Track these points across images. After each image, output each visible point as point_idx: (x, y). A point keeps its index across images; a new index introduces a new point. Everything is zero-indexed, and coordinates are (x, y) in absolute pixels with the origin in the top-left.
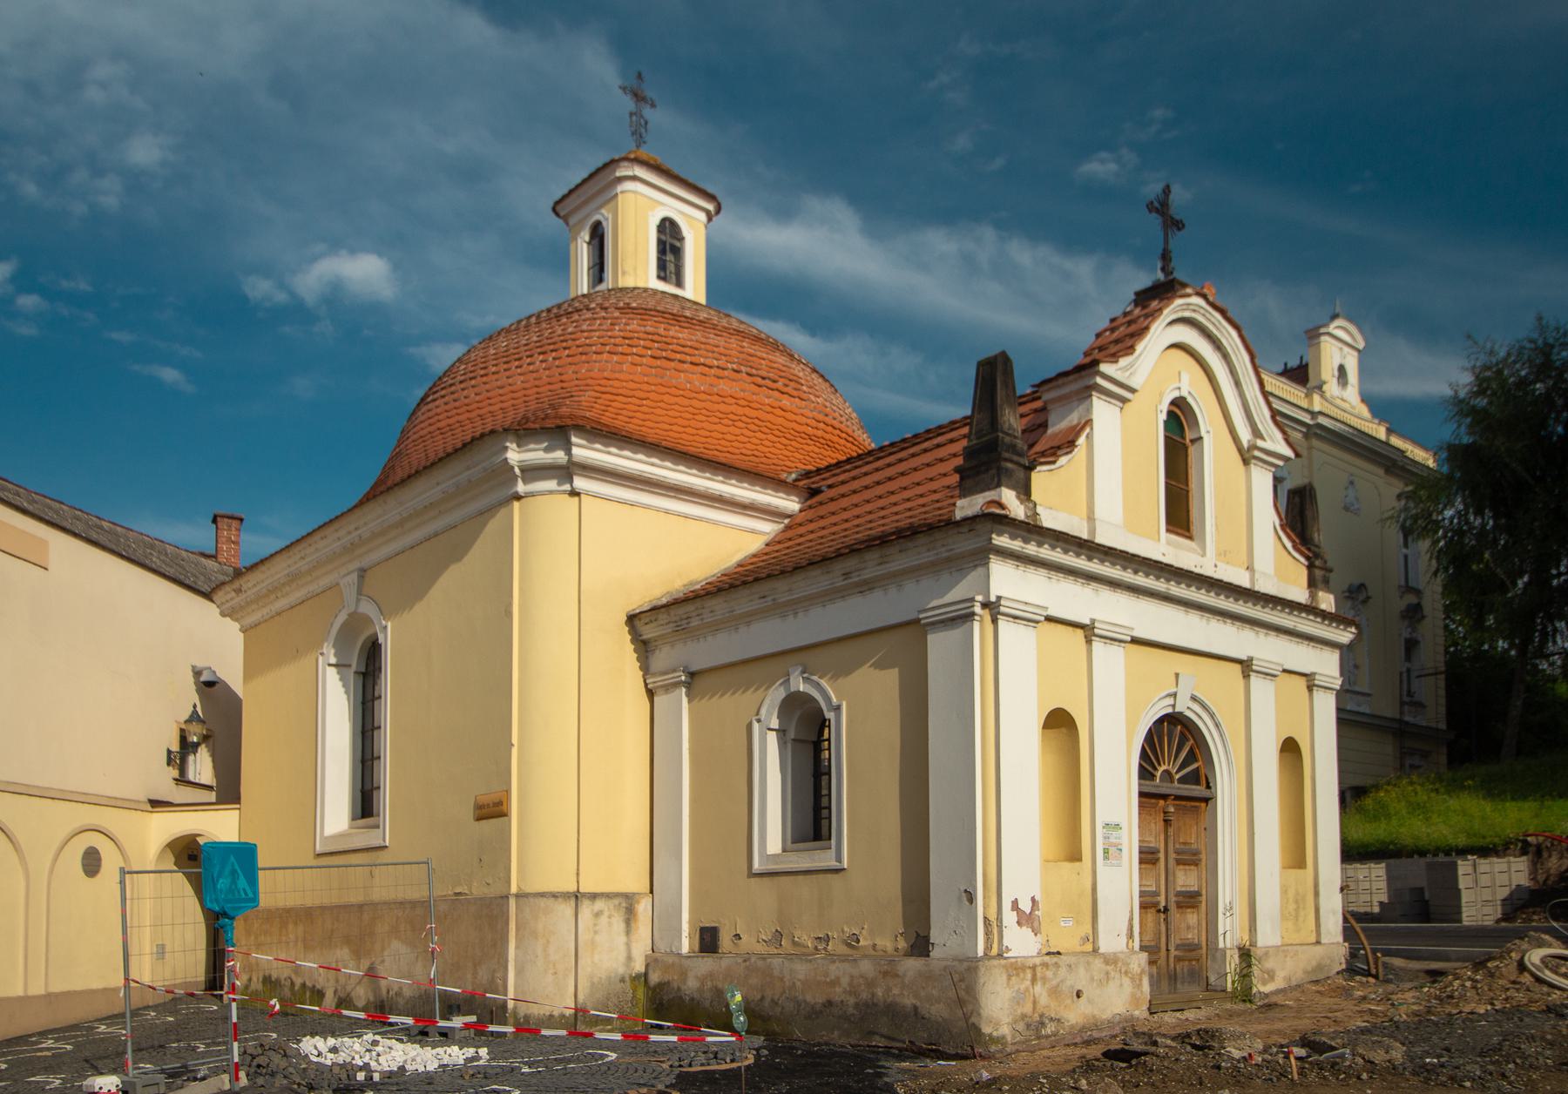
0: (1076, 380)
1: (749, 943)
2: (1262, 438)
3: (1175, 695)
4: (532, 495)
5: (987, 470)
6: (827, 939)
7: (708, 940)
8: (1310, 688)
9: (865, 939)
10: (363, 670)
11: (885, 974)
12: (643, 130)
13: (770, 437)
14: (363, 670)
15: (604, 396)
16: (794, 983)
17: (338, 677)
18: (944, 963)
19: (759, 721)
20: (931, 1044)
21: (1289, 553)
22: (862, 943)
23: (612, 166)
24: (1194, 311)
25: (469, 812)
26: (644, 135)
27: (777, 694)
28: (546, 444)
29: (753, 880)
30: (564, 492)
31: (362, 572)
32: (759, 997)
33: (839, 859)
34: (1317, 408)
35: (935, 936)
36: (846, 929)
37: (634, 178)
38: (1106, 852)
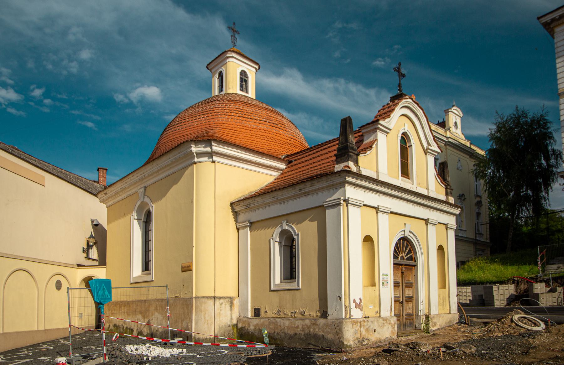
0: (372, 126)
1: (270, 314)
2: (431, 146)
3: (404, 231)
4: (200, 162)
5: (344, 156)
6: (295, 312)
7: (257, 313)
8: (447, 229)
9: (307, 312)
10: (146, 221)
11: (313, 324)
12: (235, 41)
13: (276, 143)
14: (146, 221)
15: (223, 129)
16: (284, 327)
17: (137, 223)
18: (332, 321)
19: (273, 239)
20: (328, 348)
21: (440, 184)
22: (306, 314)
23: (226, 53)
24: (409, 104)
25: (179, 270)
26: (236, 43)
27: (278, 230)
28: (204, 145)
29: (271, 292)
30: (210, 161)
31: (145, 188)
32: (273, 332)
33: (298, 286)
34: (448, 136)
35: (329, 311)
36: (301, 309)
37: (232, 57)
38: (383, 283)
